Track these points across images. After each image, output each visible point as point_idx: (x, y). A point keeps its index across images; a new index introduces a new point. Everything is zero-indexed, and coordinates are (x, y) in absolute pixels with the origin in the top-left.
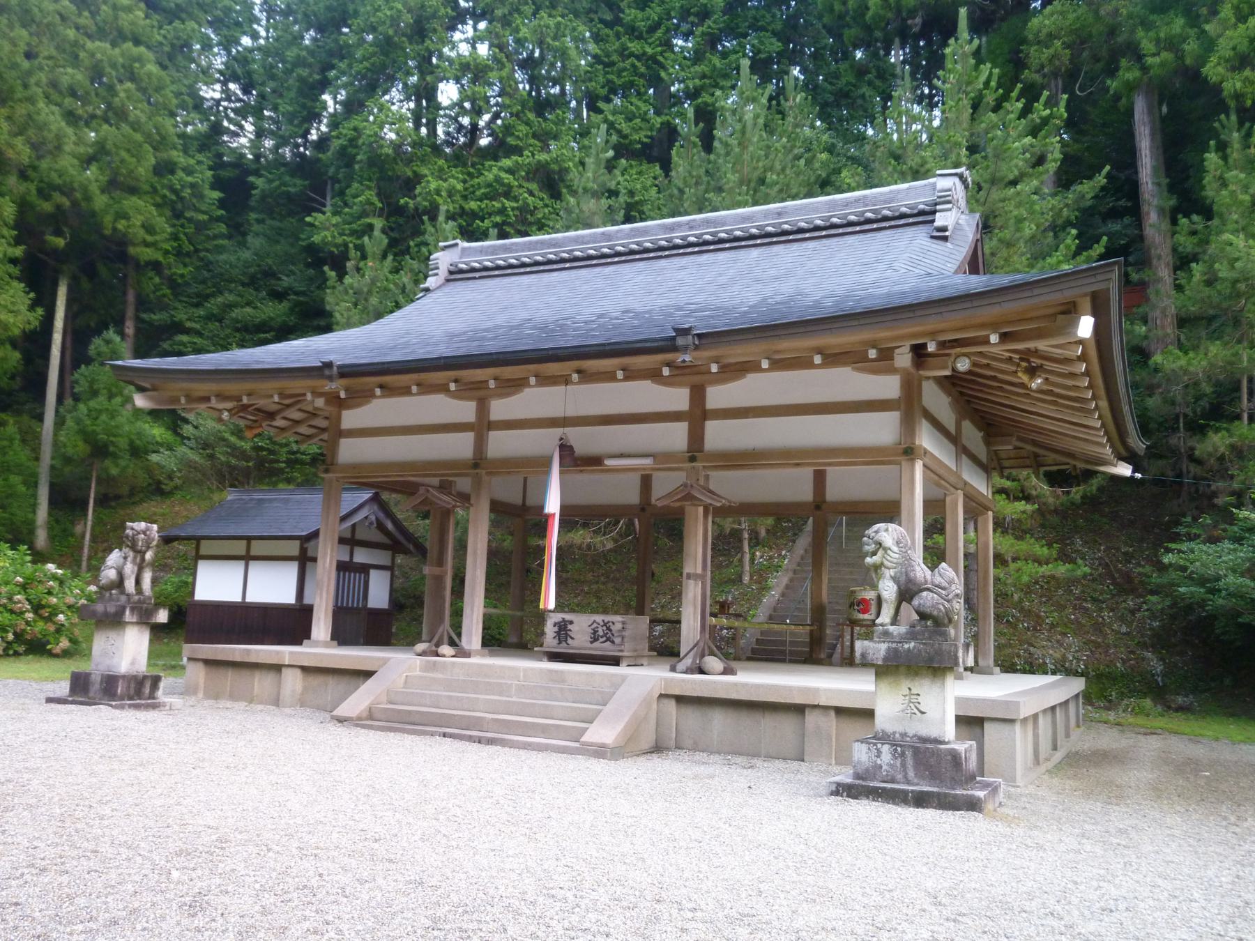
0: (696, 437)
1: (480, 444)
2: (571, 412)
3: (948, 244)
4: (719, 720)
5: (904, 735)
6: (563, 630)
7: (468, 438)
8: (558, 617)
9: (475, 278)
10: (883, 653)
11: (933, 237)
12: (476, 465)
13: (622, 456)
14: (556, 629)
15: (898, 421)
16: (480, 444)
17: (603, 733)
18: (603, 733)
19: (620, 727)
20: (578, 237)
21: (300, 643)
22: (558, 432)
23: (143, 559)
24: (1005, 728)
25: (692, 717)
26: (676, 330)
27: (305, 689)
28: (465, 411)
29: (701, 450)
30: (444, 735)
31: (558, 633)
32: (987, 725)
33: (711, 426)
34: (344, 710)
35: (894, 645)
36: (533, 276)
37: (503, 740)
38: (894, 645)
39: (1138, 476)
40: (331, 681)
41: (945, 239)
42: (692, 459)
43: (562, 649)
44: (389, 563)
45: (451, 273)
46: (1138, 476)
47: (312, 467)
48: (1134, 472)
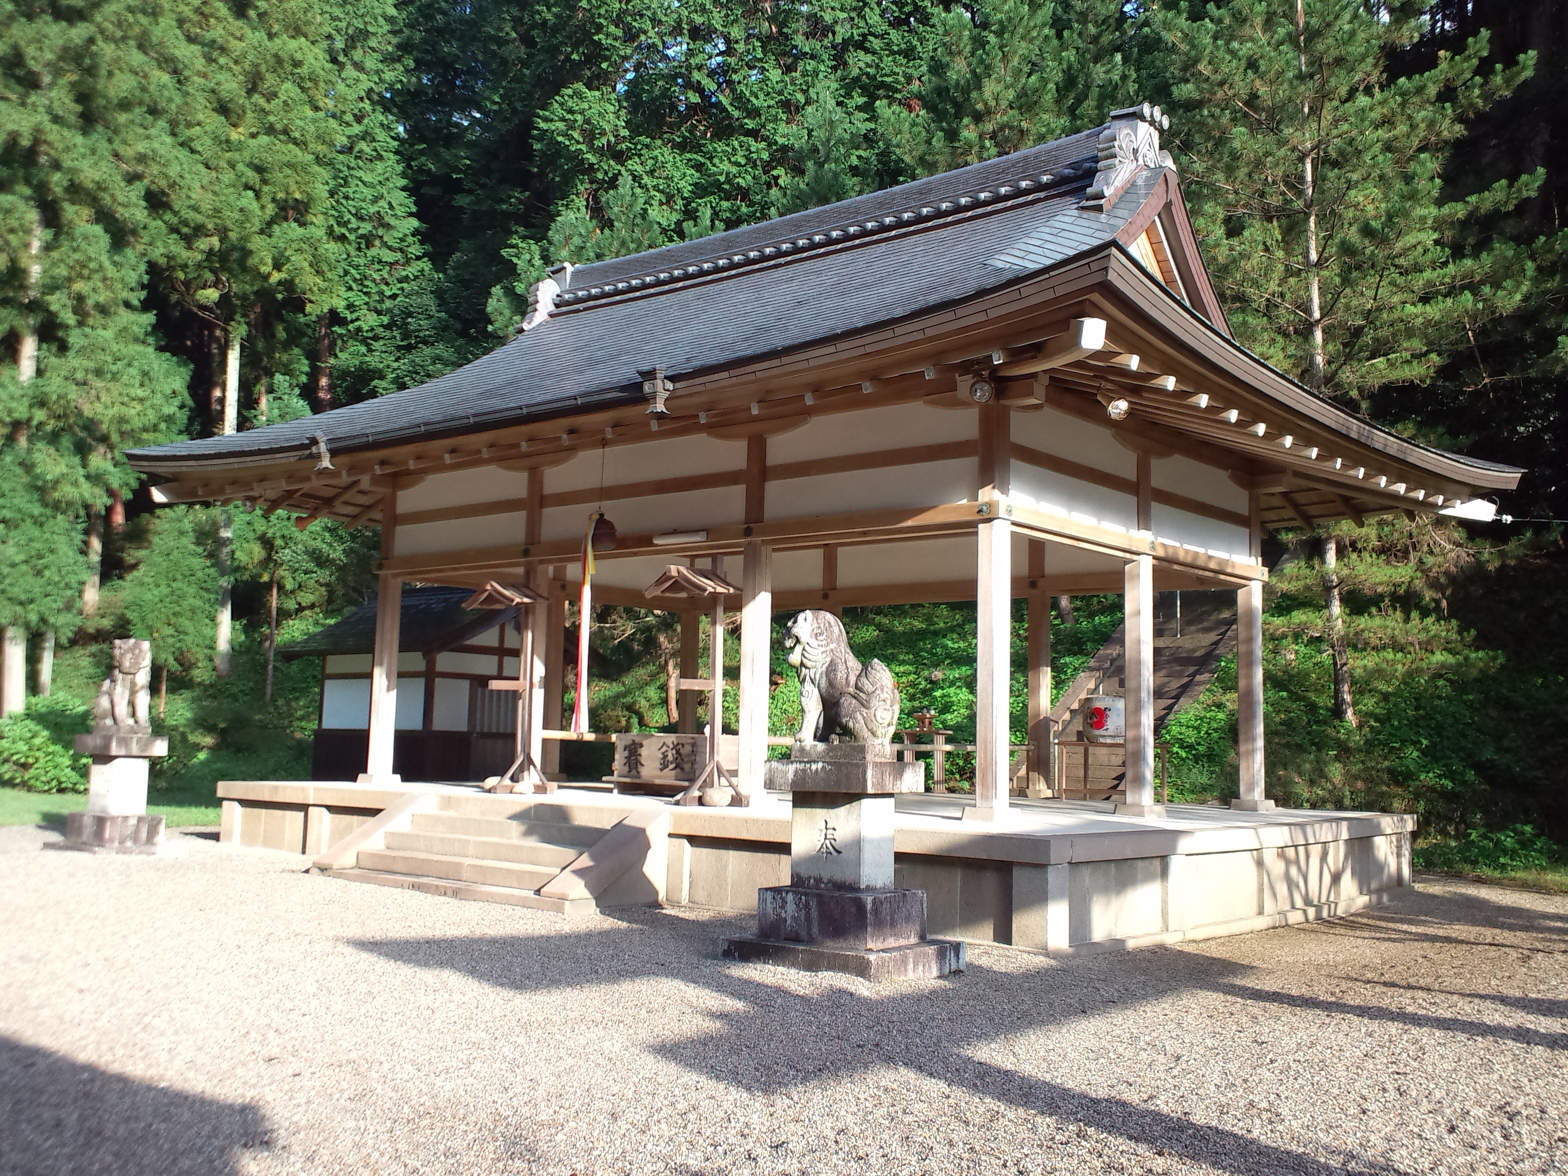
0: (755, 503)
1: (533, 525)
2: (610, 480)
3: (1103, 217)
5: (819, 880)
7: (519, 518)
9: (578, 311)
10: (790, 775)
11: (1083, 208)
13: (675, 532)
14: (626, 753)
15: (977, 466)
16: (533, 525)
21: (354, 779)
22: (591, 508)
23: (133, 684)
26: (641, 374)
28: (510, 483)
29: (760, 519)
30: (413, 887)
31: (628, 758)
32: (1016, 873)
33: (773, 487)
35: (802, 766)
37: (492, 895)
38: (802, 766)
39: (1508, 519)
41: (1099, 209)
42: (748, 532)
46: (1508, 519)
48: (1499, 512)
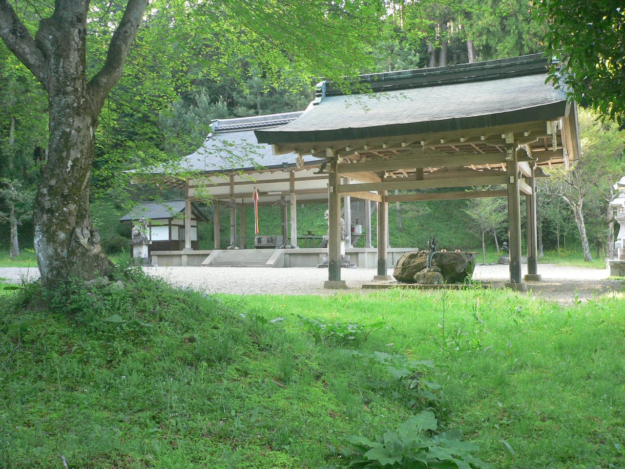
4: (299, 259)
6: (259, 240)
8: (258, 237)
12: (231, 195)
13: (273, 192)
17: (271, 262)
18: (271, 262)
19: (274, 261)
20: (256, 119)
24: (363, 254)
25: (293, 259)
27: (188, 261)
34: (204, 263)
36: (243, 132)
40: (196, 258)
43: (260, 245)
44: (196, 225)
45: (216, 130)
47: (183, 195)
